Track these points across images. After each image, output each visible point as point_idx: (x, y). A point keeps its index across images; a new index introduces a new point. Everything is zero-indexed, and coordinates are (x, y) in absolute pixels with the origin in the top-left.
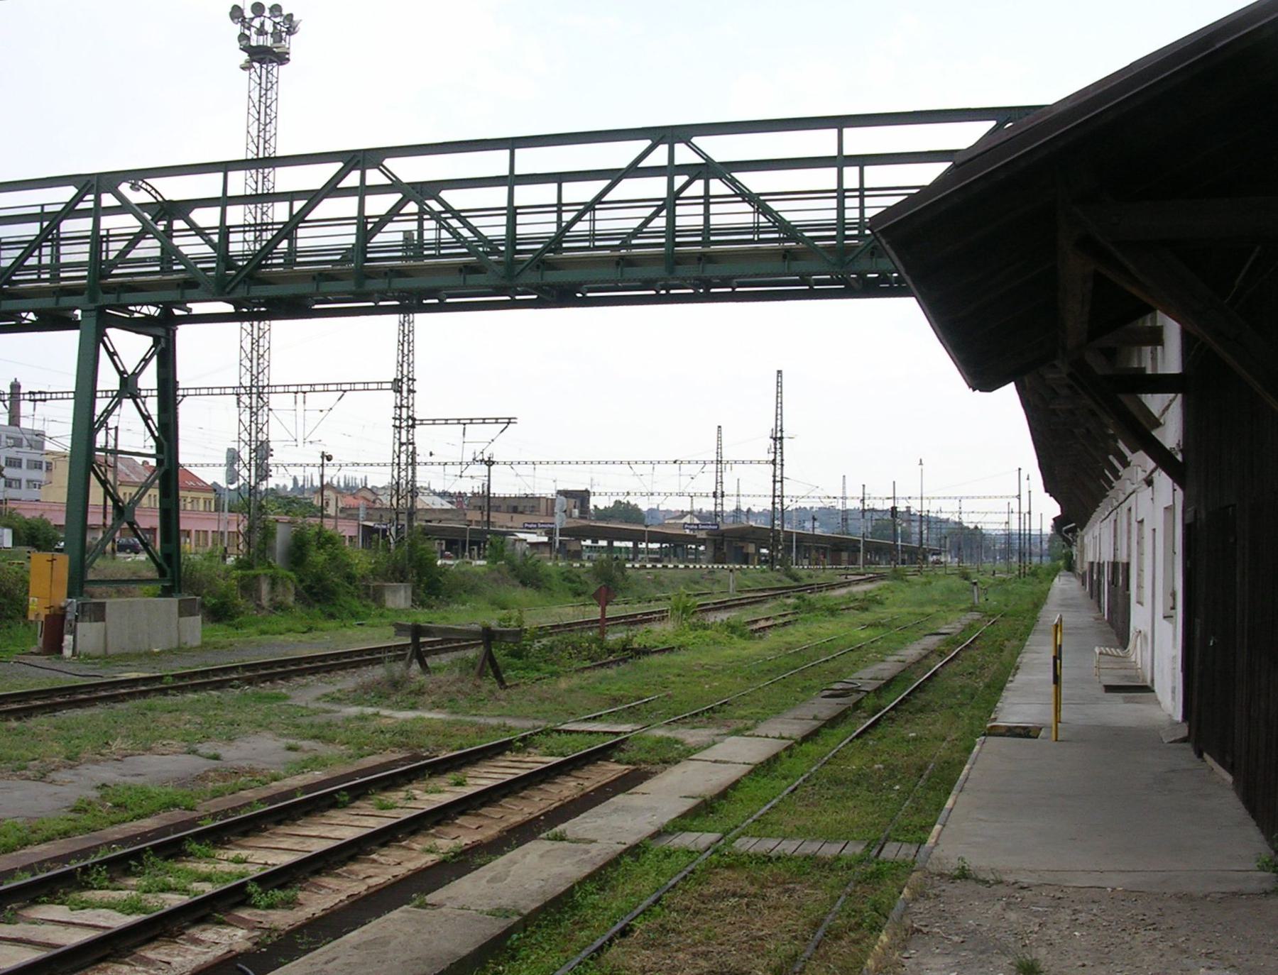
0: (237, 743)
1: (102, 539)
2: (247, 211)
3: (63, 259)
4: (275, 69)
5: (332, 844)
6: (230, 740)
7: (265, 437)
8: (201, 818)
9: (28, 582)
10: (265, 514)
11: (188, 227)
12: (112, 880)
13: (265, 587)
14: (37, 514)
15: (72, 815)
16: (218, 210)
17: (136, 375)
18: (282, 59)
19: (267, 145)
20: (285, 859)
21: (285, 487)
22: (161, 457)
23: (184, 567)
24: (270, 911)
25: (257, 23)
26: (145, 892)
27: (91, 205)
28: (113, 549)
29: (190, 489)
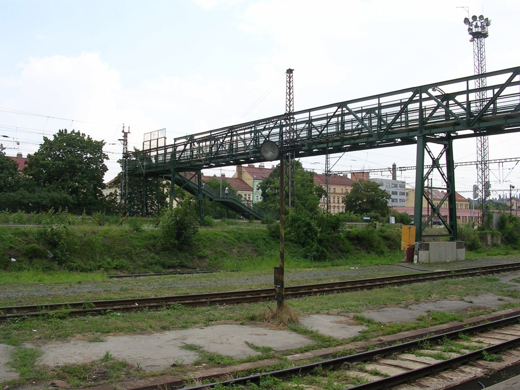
0: (479, 297)
1: (428, 220)
2: (477, 95)
3: (410, 119)
4: (483, 40)
5: (516, 338)
6: (477, 296)
7: (488, 180)
8: (465, 325)
9: (401, 236)
10: (489, 209)
11: (455, 103)
12: (431, 346)
13: (489, 238)
14: (404, 212)
15: (417, 322)
16: (465, 95)
17: (438, 159)
18: (485, 35)
19: (482, 69)
20: (498, 343)
21: (496, 199)
22: (449, 189)
23: (458, 231)
24: (491, 362)
25: (474, 23)
26: (444, 351)
27: (418, 98)
28: (431, 224)
29: (459, 201)
